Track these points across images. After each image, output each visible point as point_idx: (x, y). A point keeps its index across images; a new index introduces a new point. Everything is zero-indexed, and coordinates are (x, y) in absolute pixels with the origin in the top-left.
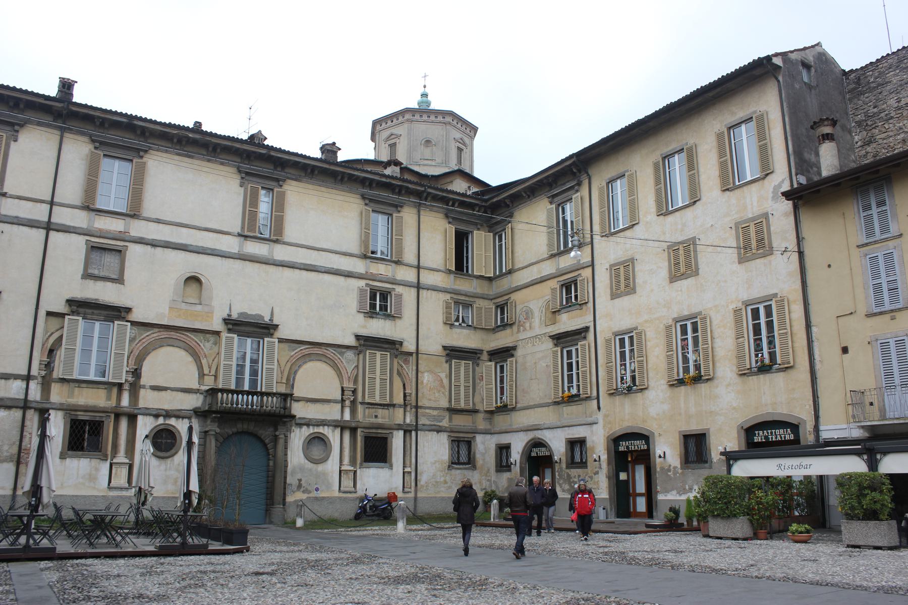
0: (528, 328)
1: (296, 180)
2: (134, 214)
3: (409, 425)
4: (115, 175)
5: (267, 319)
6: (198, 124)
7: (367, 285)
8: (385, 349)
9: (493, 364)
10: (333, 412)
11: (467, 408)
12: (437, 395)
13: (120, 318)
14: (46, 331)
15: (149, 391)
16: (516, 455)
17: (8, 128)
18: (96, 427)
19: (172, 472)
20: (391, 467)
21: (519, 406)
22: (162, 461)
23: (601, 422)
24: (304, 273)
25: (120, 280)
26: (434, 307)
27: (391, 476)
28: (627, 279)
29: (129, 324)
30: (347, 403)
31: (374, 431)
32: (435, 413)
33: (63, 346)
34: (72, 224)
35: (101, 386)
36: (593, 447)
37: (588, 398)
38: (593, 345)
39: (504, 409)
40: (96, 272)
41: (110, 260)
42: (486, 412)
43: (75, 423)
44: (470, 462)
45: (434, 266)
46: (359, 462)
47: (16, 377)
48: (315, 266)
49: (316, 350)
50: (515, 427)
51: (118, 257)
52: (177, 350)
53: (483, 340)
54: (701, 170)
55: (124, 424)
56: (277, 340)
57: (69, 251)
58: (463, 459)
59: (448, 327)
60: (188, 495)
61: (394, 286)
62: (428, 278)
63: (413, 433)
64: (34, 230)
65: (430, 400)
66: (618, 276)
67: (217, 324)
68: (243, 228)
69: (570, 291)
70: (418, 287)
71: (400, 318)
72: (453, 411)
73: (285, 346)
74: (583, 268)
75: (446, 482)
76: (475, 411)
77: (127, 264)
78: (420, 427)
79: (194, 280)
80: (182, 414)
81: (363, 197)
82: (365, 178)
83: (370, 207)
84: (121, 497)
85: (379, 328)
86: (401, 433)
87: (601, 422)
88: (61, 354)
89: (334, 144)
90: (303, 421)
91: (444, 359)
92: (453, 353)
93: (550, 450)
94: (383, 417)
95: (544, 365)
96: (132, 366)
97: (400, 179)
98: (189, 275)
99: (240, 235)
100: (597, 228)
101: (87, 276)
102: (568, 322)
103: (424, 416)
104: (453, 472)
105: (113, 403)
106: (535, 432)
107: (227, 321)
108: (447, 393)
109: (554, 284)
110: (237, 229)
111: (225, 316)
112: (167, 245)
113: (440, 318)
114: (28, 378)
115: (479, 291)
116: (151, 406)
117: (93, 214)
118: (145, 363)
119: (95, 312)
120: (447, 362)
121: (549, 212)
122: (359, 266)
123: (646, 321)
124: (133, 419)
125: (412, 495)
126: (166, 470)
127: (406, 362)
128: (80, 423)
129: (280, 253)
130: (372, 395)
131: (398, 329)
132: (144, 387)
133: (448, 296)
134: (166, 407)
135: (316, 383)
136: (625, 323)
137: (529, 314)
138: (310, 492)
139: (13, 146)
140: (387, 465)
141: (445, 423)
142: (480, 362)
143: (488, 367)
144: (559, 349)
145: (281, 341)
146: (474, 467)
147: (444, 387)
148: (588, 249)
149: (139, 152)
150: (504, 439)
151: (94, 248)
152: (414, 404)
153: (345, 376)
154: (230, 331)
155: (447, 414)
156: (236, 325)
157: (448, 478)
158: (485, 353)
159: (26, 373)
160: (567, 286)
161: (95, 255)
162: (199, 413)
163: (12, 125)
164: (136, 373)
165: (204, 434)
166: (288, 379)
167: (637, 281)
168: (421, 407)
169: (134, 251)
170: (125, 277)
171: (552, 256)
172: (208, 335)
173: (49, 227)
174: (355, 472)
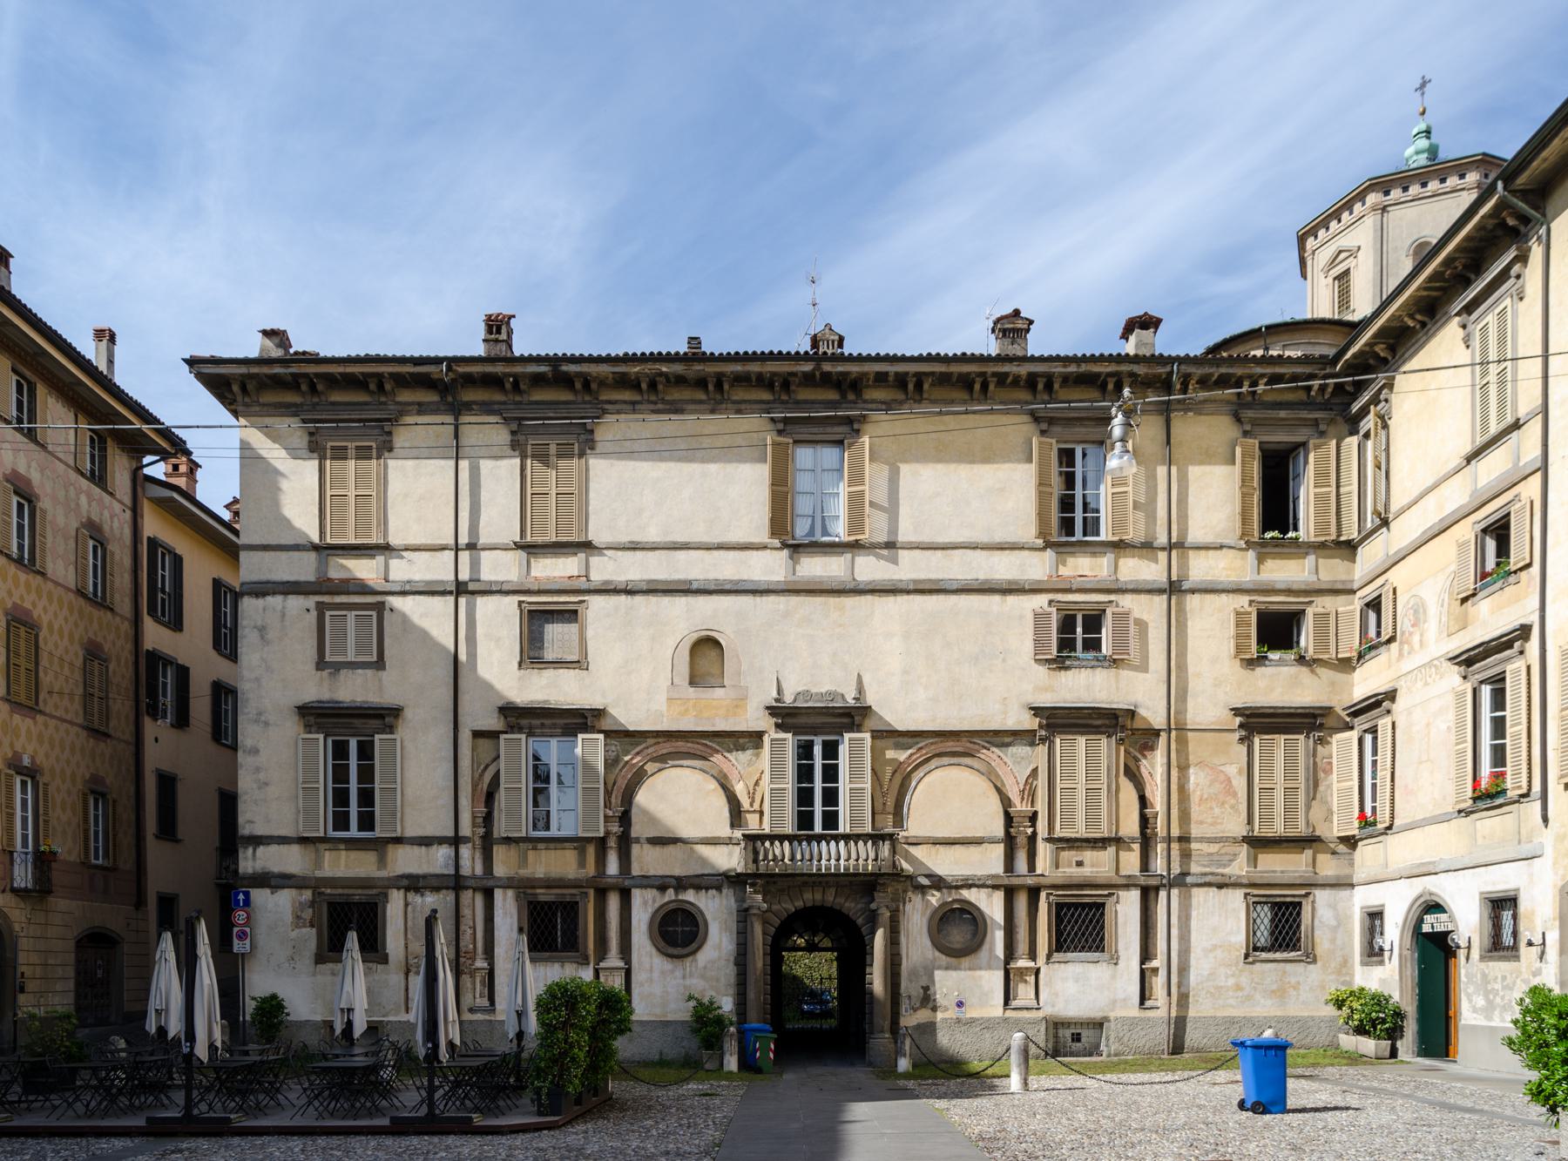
0: (1417, 646)
7: (1050, 602)
11: (1292, 833)
12: (1217, 811)
13: (586, 728)
14: (474, 761)
15: (647, 847)
18: (571, 910)
19: (695, 981)
21: (1397, 822)
22: (678, 962)
23: (1549, 851)
27: (1113, 977)
32: (1214, 848)
33: (502, 786)
47: (441, 841)
48: (1015, 582)
55: (613, 903)
56: (867, 736)
57: (498, 623)
60: (520, 1035)
61: (1112, 597)
62: (1201, 568)
64: (437, 600)
72: (1258, 844)
75: (1238, 987)
76: (1310, 841)
85: (1085, 686)
88: (502, 797)
89: (1017, 313)
92: (1257, 722)
93: (1452, 919)
94: (1097, 864)
95: (1444, 727)
97: (999, 359)
98: (695, 636)
102: (1493, 616)
105: (591, 870)
109: (1466, 531)
114: (456, 841)
116: (652, 873)
122: (1038, 566)
124: (625, 895)
126: (684, 977)
128: (550, 908)
130: (1069, 821)
131: (1138, 690)
132: (637, 840)
133: (1243, 601)
134: (677, 872)
137: (1419, 611)
140: (1106, 955)
141: (1239, 867)
147: (1235, 794)
157: (1244, 980)
159: (451, 834)
164: (625, 819)
169: (596, 603)
174: (1038, 971)
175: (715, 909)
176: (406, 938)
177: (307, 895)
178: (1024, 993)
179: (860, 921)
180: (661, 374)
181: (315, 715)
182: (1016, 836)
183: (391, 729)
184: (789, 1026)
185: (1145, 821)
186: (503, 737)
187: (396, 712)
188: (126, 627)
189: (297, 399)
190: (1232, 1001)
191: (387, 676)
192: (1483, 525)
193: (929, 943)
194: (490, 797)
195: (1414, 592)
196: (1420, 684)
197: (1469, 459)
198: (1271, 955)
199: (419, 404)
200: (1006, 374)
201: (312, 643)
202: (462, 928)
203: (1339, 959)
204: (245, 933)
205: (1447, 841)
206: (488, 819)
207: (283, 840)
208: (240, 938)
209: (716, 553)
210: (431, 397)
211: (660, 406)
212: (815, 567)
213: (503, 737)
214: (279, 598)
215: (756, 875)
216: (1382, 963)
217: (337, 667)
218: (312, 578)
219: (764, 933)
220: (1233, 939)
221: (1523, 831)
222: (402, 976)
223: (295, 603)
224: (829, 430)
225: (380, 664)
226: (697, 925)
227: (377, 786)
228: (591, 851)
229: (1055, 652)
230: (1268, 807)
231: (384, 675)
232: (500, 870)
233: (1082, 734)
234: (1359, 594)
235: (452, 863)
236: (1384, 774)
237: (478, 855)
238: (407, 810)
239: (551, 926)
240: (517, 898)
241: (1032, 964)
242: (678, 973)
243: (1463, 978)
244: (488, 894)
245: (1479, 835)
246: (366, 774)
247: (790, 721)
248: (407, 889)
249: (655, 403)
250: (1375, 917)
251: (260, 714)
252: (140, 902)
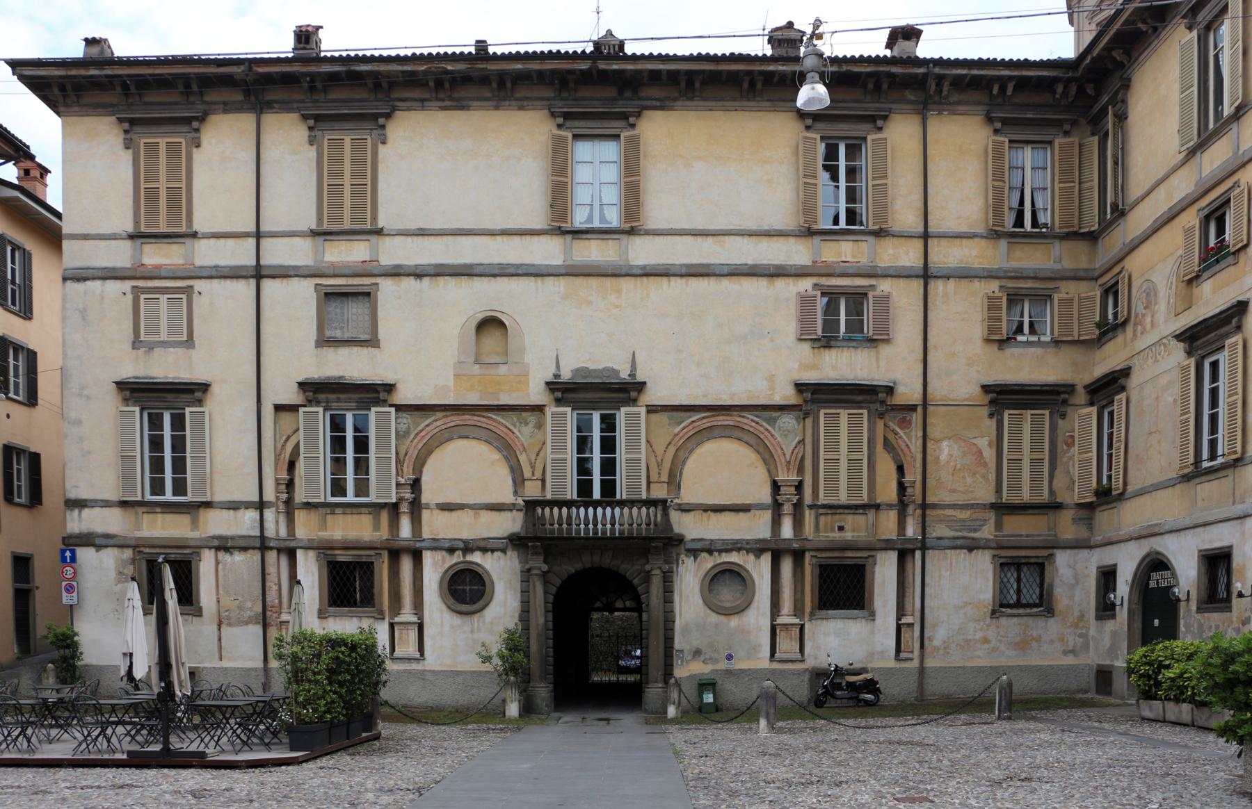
0: (1148, 326)
1: (662, 108)
2: (631, 228)
3: (910, 540)
4: (596, 166)
5: (624, 375)
6: (481, 45)
7: (815, 286)
8: (858, 405)
9: (1093, 410)
10: (758, 527)
11: (1037, 500)
12: (969, 480)
15: (436, 512)
17: (369, 125)
18: (367, 568)
20: (872, 616)
21: (1130, 489)
22: (467, 619)
24: (694, 282)
25: (372, 342)
26: (961, 315)
29: (393, 410)
30: (787, 508)
31: (836, 554)
33: (302, 456)
34: (292, 263)
35: (363, 510)
40: (338, 334)
41: (355, 310)
42: (1080, 506)
43: (334, 567)
45: (963, 229)
46: (808, 609)
47: (248, 505)
48: (708, 265)
50: (1124, 532)
51: (367, 305)
52: (473, 443)
53: (1075, 364)
55: (406, 565)
56: (643, 410)
57: (293, 304)
58: (1030, 594)
59: (995, 347)
63: (918, 554)
65: (954, 491)
67: (535, 393)
71: (888, 341)
72: (1002, 509)
76: (1054, 507)
77: (380, 314)
78: (929, 543)
79: (490, 324)
80: (491, 544)
82: (553, 72)
83: (817, 131)
84: (410, 672)
86: (893, 557)
88: (301, 465)
90: (698, 545)
91: (985, 411)
92: (1003, 397)
93: (1174, 575)
94: (855, 529)
95: (1170, 399)
96: (409, 475)
98: (480, 316)
101: (324, 341)
102: (1213, 297)
103: (940, 521)
104: (1003, 621)
105: (384, 533)
106: (1153, 540)
107: (552, 386)
108: (992, 476)
109: (1191, 218)
111: (550, 378)
112: (664, 272)
113: (977, 330)
114: (261, 506)
115: (1068, 264)
117: (569, 237)
118: (425, 470)
119: (343, 396)
120: (991, 415)
122: (798, 253)
124: (417, 556)
126: (472, 631)
127: (905, 424)
128: (348, 567)
129: (642, 252)
131: (892, 365)
132: (428, 507)
133: (994, 286)
135: (723, 477)
138: (716, 661)
139: (197, 155)
140: (864, 613)
142: (1069, 410)
143: (1084, 417)
145: (652, 409)
146: (1050, 612)
147: (985, 465)
149: (627, 119)
151: (330, 296)
152: (919, 501)
153: (781, 462)
154: (559, 402)
155: (991, 516)
157: (991, 634)
158: (1080, 390)
159: (256, 499)
161: (334, 307)
162: (516, 542)
163: (375, 116)
164: (416, 485)
165: (526, 575)
168: (934, 506)
169: (387, 288)
170: (380, 336)
172: (524, 414)
173: (259, 274)
174: (802, 627)
175: (501, 570)
176: (218, 593)
177: (128, 553)
178: (787, 645)
179: (636, 581)
180: (447, 72)
181: (133, 390)
183: (200, 402)
185: (902, 487)
186: (302, 410)
187: (205, 387)
189: (114, 100)
190: (979, 653)
191: (197, 354)
192: (1206, 212)
193: (701, 601)
194: (292, 465)
195: (1146, 277)
196: (1150, 361)
197: (1192, 153)
198: (1015, 611)
199: (225, 103)
200: (772, 73)
202: (268, 584)
203: (1077, 614)
204: (72, 587)
207: (106, 504)
208: (68, 591)
209: (499, 238)
211: (447, 103)
212: (593, 252)
213: (302, 410)
214: (98, 283)
215: (535, 539)
216: (1113, 617)
217: (151, 347)
218: (128, 265)
219: (546, 592)
220: (982, 597)
221: (1237, 493)
222: (215, 627)
223: (113, 287)
224: (606, 124)
225: (189, 342)
226: (484, 584)
227: (188, 455)
228: (385, 516)
229: (820, 332)
230: (1016, 477)
231: (193, 353)
232: (301, 532)
233: (846, 408)
234: (1101, 281)
235: (257, 525)
236: (1119, 445)
237: (282, 519)
238: (216, 477)
239: (348, 583)
240: (318, 558)
241: (797, 621)
242: (467, 628)
243: (1182, 628)
244: (291, 554)
245: (1199, 498)
246: (179, 444)
247: (570, 396)
248: (218, 549)
249: (443, 100)
250: (1108, 576)
251: (83, 388)
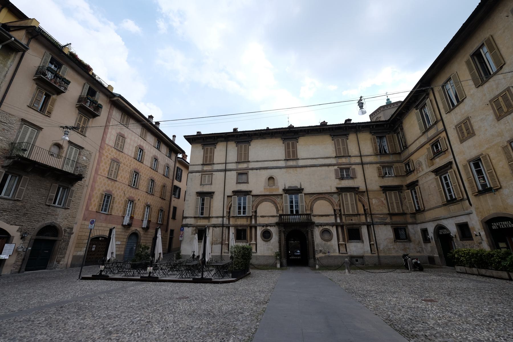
5: (299, 187)
8: (351, 192)
9: (409, 191)
10: (332, 220)
11: (399, 212)
16: (431, 234)
18: (245, 231)
21: (426, 209)
23: (474, 212)
26: (372, 172)
28: (467, 129)
32: (382, 216)
36: (474, 227)
37: (462, 200)
38: (457, 171)
39: (419, 211)
40: (240, 181)
41: (244, 177)
44: (408, 239)
45: (369, 154)
47: (220, 217)
49: (321, 196)
54: (500, 46)
57: (232, 176)
62: (366, 160)
63: (372, 226)
66: (461, 130)
67: (280, 192)
68: (286, 157)
69: (437, 148)
70: (362, 164)
72: (391, 215)
73: (308, 196)
74: (441, 133)
75: (394, 249)
76: (404, 214)
81: (331, 135)
85: (243, 187)
87: (474, 212)
88: (232, 208)
91: (382, 192)
92: (385, 189)
94: (355, 220)
99: (285, 160)
100: (442, 111)
101: (238, 183)
102: (440, 162)
105: (249, 223)
106: (438, 221)
108: (387, 207)
109: (428, 146)
110: (284, 158)
113: (376, 175)
114: (223, 217)
115: (395, 159)
120: (383, 193)
121: (416, 114)
123: (488, 149)
124: (256, 228)
125: (376, 255)
127: (363, 195)
129: (301, 163)
131: (358, 183)
134: (266, 223)
135: (322, 208)
136: (474, 154)
137: (420, 164)
141: (388, 220)
143: (407, 193)
144: (438, 177)
145: (305, 194)
148: (441, 123)
150: (424, 226)
151: (239, 174)
154: (285, 193)
156: (287, 191)
157: (395, 246)
160: (435, 145)
161: (240, 176)
162: (277, 224)
164: (256, 212)
165: (280, 232)
166: (311, 208)
167: (474, 128)
168: (374, 214)
169: (250, 172)
171: (424, 133)
174: (346, 244)
175: (274, 230)
182: (337, 213)
184: (481, 50)
185: (365, 210)
188: (171, 181)
201: (200, 181)
205: (441, 212)
206: (229, 212)
207: (191, 217)
210: (223, 139)
215: (282, 223)
217: (204, 185)
223: (198, 174)
225: (211, 184)
228: (249, 219)
232: (231, 223)
239: (241, 234)
248: (213, 227)
252: (167, 231)
